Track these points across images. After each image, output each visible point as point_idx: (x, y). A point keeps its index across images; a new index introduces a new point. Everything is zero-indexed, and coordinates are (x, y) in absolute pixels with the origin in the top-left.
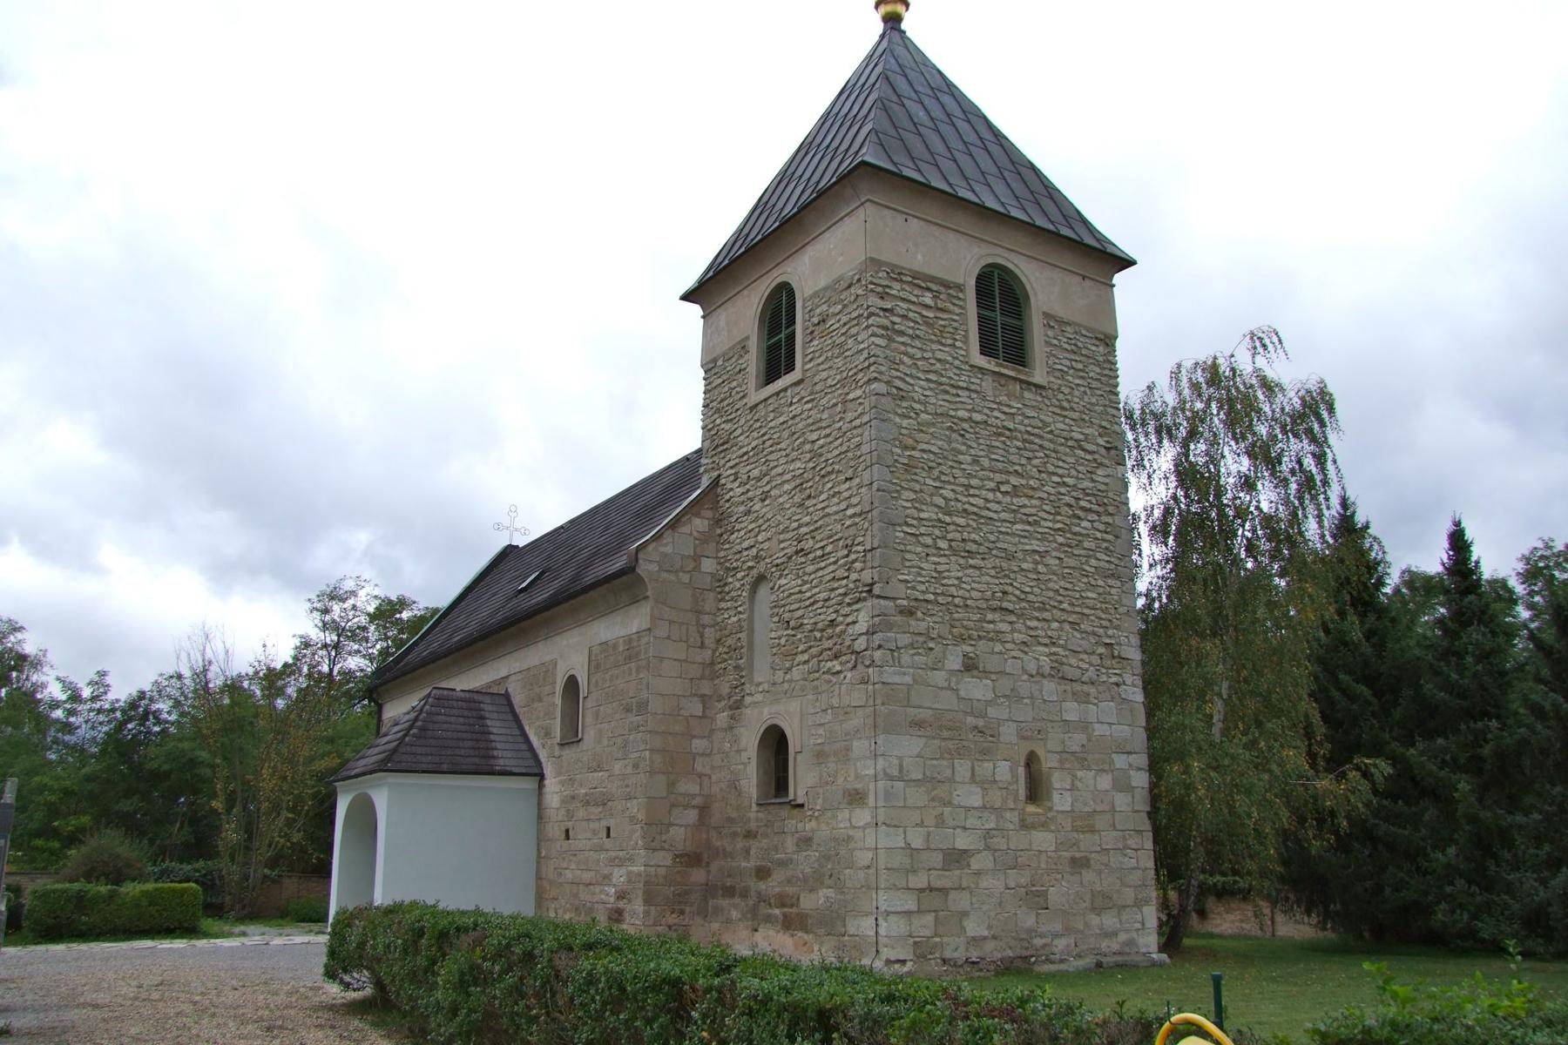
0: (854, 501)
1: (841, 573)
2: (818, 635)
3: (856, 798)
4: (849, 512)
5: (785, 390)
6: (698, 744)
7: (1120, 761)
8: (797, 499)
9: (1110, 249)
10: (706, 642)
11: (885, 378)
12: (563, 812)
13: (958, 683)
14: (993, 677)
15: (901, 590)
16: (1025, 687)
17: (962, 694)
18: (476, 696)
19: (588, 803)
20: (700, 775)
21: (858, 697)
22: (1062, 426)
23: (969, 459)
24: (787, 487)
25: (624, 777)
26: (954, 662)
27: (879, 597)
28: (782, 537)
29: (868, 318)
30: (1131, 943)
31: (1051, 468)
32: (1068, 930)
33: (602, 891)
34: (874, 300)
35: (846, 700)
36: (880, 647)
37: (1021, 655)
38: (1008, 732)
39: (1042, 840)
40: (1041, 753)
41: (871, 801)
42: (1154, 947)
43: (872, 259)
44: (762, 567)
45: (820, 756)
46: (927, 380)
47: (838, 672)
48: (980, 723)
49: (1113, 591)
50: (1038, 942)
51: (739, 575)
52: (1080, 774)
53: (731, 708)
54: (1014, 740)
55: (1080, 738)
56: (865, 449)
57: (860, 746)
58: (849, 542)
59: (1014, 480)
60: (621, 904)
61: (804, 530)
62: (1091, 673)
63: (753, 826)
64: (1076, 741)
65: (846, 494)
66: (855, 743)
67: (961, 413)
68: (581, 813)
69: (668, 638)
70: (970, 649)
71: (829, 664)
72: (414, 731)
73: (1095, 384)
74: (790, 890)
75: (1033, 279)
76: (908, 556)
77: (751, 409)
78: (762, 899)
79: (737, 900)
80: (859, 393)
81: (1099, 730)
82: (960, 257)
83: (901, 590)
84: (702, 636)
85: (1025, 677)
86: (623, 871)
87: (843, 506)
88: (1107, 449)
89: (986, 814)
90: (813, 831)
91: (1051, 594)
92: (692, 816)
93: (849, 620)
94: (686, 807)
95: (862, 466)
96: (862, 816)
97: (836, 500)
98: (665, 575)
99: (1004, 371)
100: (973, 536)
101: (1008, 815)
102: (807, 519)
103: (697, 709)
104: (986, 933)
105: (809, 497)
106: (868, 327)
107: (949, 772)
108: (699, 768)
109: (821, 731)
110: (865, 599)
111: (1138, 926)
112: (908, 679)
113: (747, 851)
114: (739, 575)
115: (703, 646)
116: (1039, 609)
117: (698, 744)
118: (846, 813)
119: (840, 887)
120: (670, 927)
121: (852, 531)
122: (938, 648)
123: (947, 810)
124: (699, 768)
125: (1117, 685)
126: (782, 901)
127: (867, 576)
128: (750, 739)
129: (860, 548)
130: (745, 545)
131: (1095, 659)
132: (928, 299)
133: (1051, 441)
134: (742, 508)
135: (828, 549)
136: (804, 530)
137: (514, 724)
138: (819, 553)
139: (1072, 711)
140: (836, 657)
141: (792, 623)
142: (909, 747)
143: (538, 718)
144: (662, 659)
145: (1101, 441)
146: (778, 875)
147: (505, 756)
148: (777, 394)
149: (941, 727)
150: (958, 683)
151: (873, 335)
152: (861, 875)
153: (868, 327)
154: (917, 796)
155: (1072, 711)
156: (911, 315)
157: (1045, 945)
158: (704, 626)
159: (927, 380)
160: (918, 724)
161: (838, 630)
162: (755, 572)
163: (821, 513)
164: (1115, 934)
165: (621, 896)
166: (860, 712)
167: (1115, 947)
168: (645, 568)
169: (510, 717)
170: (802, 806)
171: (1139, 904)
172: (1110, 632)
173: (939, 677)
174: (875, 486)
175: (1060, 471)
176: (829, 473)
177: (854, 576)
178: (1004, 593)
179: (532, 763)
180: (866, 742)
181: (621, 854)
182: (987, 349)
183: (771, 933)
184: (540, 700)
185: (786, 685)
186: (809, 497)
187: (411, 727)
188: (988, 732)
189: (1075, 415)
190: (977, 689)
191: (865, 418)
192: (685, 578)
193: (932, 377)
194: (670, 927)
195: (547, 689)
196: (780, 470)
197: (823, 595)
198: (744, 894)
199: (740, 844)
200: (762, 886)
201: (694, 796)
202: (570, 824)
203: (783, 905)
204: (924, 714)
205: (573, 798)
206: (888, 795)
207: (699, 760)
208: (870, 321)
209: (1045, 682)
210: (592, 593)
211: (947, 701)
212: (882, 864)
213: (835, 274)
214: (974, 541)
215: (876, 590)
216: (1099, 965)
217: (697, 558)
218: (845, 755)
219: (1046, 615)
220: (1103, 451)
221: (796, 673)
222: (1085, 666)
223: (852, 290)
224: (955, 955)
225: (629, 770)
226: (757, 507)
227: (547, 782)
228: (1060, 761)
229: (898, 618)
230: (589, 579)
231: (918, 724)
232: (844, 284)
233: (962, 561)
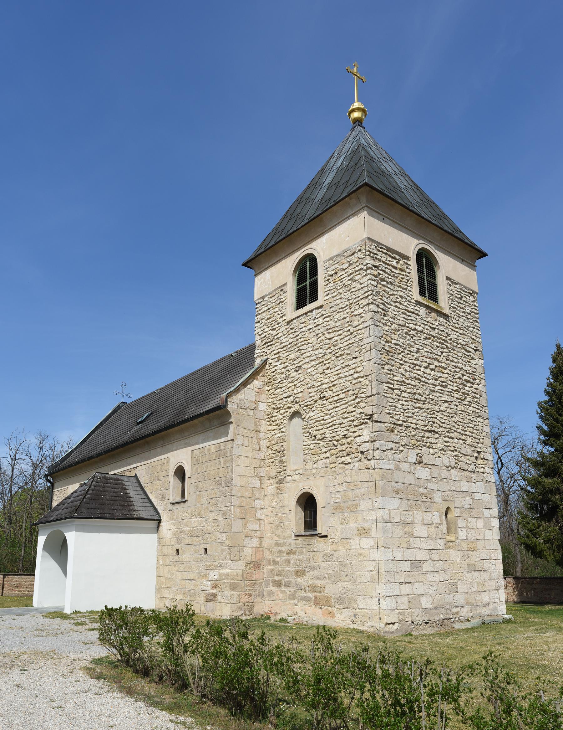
0: (359, 369)
1: (351, 409)
2: (336, 443)
3: (364, 532)
4: (356, 376)
5: (311, 311)
6: (258, 503)
7: (487, 513)
8: (320, 369)
9: (476, 247)
10: (262, 447)
11: (377, 303)
12: (174, 540)
13: (415, 469)
14: (430, 467)
15: (388, 419)
16: (444, 474)
17: (417, 475)
18: (119, 477)
19: (191, 535)
20: (259, 520)
21: (364, 475)
22: (456, 337)
23: (415, 350)
24: (313, 363)
25: (215, 521)
26: (413, 458)
27: (376, 421)
28: (310, 390)
29: (366, 270)
30: (495, 609)
31: (451, 358)
32: (468, 604)
33: (202, 584)
34: (369, 260)
35: (355, 478)
36: (378, 449)
37: (442, 456)
38: (437, 497)
39: (455, 555)
40: (452, 508)
41: (374, 534)
42: (504, 612)
43: (369, 238)
44: (297, 407)
45: (338, 509)
46: (396, 306)
47: (349, 463)
48: (425, 491)
49: (480, 424)
50: (455, 610)
51: (282, 412)
52: (470, 519)
53: (277, 483)
54: (440, 501)
55: (469, 501)
56: (366, 341)
57: (364, 505)
58: (356, 392)
59: (437, 363)
60: (215, 591)
61: (324, 386)
62: (472, 466)
63: (293, 547)
64: (467, 503)
65: (354, 366)
66: (361, 502)
67: (411, 326)
68: (187, 540)
69: (242, 445)
70: (419, 452)
71: (343, 459)
72: (88, 496)
73: (469, 317)
74: (319, 583)
75: (440, 257)
76: (389, 400)
77: (288, 323)
78: (299, 588)
79: (283, 588)
80: (361, 311)
81: (477, 496)
82: (410, 245)
83: (388, 419)
84: (259, 445)
85: (444, 468)
86: (216, 573)
87: (352, 372)
88: (475, 351)
89: (429, 541)
90: (334, 550)
91: (454, 424)
92: (255, 541)
93: (356, 434)
94: (252, 537)
95: (364, 351)
96: (367, 542)
97: (346, 369)
98: (240, 410)
99: (431, 305)
100: (418, 391)
101: (439, 541)
102: (327, 380)
103: (257, 483)
104: (431, 606)
105: (328, 368)
106: (366, 275)
107: (412, 517)
108: (258, 516)
109: (338, 495)
110: (366, 423)
111: (497, 600)
112: (392, 467)
113: (289, 561)
114: (282, 412)
115: (260, 450)
116: (448, 432)
117: (258, 503)
118: (357, 541)
119: (353, 581)
120: (244, 604)
121: (358, 386)
122: (405, 450)
123: (412, 539)
124: (258, 516)
125: (483, 473)
126: (314, 589)
127: (368, 410)
128: (291, 499)
129: (363, 395)
130: (285, 395)
131: (473, 459)
132: (394, 263)
133: (451, 344)
134: (283, 376)
135: (341, 396)
136: (324, 386)
137: (142, 493)
138: (336, 398)
139: (465, 486)
140: (348, 455)
141: (318, 437)
142: (394, 503)
143: (157, 489)
144: (239, 456)
145: (472, 346)
146: (310, 574)
147: (141, 509)
148: (306, 314)
149: (407, 494)
150: (415, 469)
151: (371, 279)
152: (368, 575)
153: (366, 275)
154: (398, 531)
155: (465, 486)
156: (386, 270)
157: (458, 612)
158: (260, 439)
159: (396, 306)
160: (397, 492)
161: (349, 440)
162: (292, 410)
163: (337, 377)
164: (487, 605)
165: (215, 586)
166: (365, 485)
167: (488, 612)
168: (231, 407)
169: (139, 489)
170: (326, 536)
171: (497, 589)
172: (480, 445)
173: (405, 467)
174: (373, 361)
175: (456, 360)
176: (341, 355)
177: (359, 411)
178: (434, 423)
179: (154, 513)
180: (370, 501)
181: (215, 563)
182: (422, 293)
183: (307, 607)
184: (158, 480)
185: (314, 471)
186: (328, 368)
187: (86, 494)
188: (429, 496)
189: (461, 332)
190: (423, 473)
191: (366, 324)
192: (251, 413)
193: (397, 304)
194: (244, 604)
195: (164, 473)
196: (308, 354)
197: (340, 421)
198: (287, 585)
199: (285, 557)
200: (299, 580)
201: (256, 531)
202: (179, 547)
203: (314, 592)
204: (400, 486)
205: (181, 532)
206: (385, 530)
207: (259, 512)
208: (368, 271)
209: (452, 470)
210: (195, 421)
211: (410, 479)
212: (382, 569)
213: (344, 247)
214: (419, 394)
215: (375, 417)
216: (483, 623)
217: (256, 402)
218: (355, 510)
219: (451, 435)
220: (473, 351)
221: (321, 464)
222: (470, 463)
223: (355, 255)
224: (418, 618)
225: (220, 516)
226: (292, 375)
227: (162, 524)
228: (461, 513)
229: (387, 433)
230: (191, 413)
231: (397, 492)
232: (349, 253)
233: (414, 404)
